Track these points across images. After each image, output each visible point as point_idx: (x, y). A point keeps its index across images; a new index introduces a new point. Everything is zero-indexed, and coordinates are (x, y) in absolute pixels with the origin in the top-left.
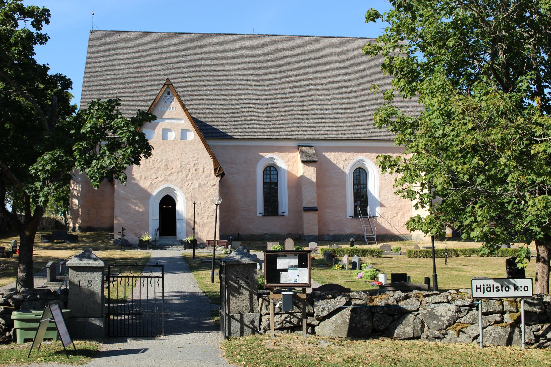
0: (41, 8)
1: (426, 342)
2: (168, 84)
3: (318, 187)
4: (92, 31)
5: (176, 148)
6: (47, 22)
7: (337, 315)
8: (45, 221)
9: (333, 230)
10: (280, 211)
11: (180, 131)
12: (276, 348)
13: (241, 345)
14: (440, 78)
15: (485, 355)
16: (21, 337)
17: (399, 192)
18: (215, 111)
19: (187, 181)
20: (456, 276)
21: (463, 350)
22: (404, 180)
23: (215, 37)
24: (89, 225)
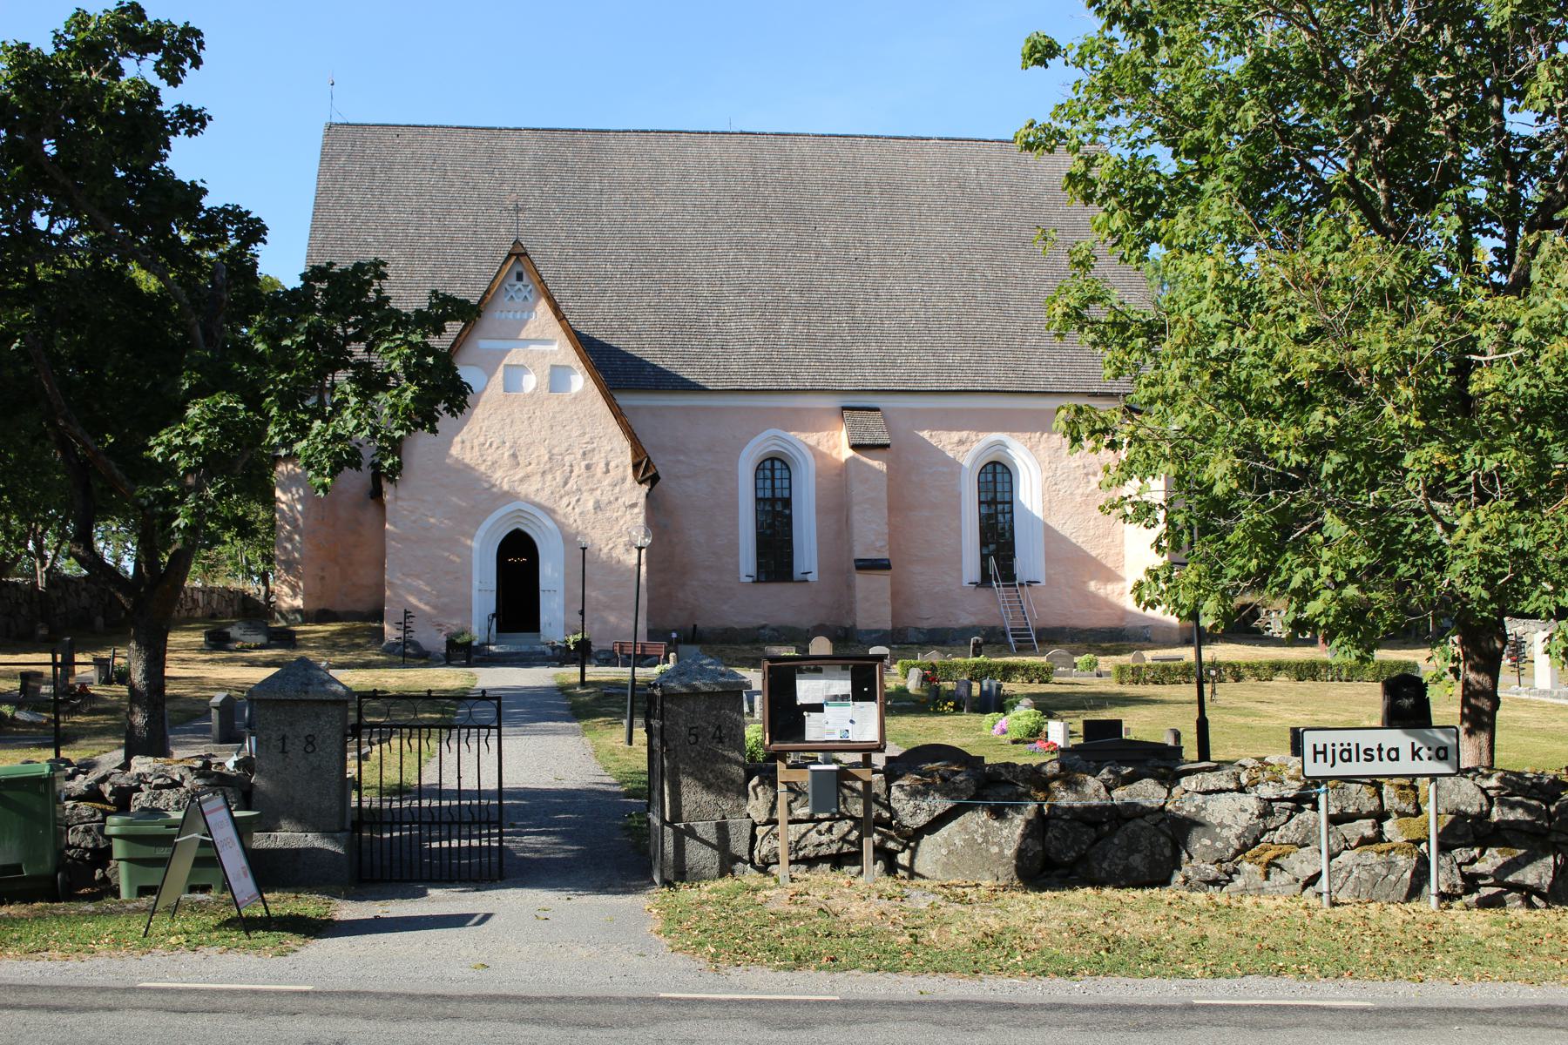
0: (180, 25)
1: (1185, 893)
2: (518, 254)
3: (890, 509)
4: (330, 127)
5: (538, 413)
6: (197, 62)
7: (953, 824)
8: (215, 596)
9: (929, 616)
10: (797, 574)
11: (547, 371)
12: (794, 910)
13: (702, 903)
14: (1218, 204)
15: (1339, 925)
16: (130, 884)
17: (1113, 507)
18: (635, 321)
19: (567, 494)
20: (1241, 727)
21: (1282, 912)
22: (1127, 470)
23: (634, 138)
24: (322, 605)
